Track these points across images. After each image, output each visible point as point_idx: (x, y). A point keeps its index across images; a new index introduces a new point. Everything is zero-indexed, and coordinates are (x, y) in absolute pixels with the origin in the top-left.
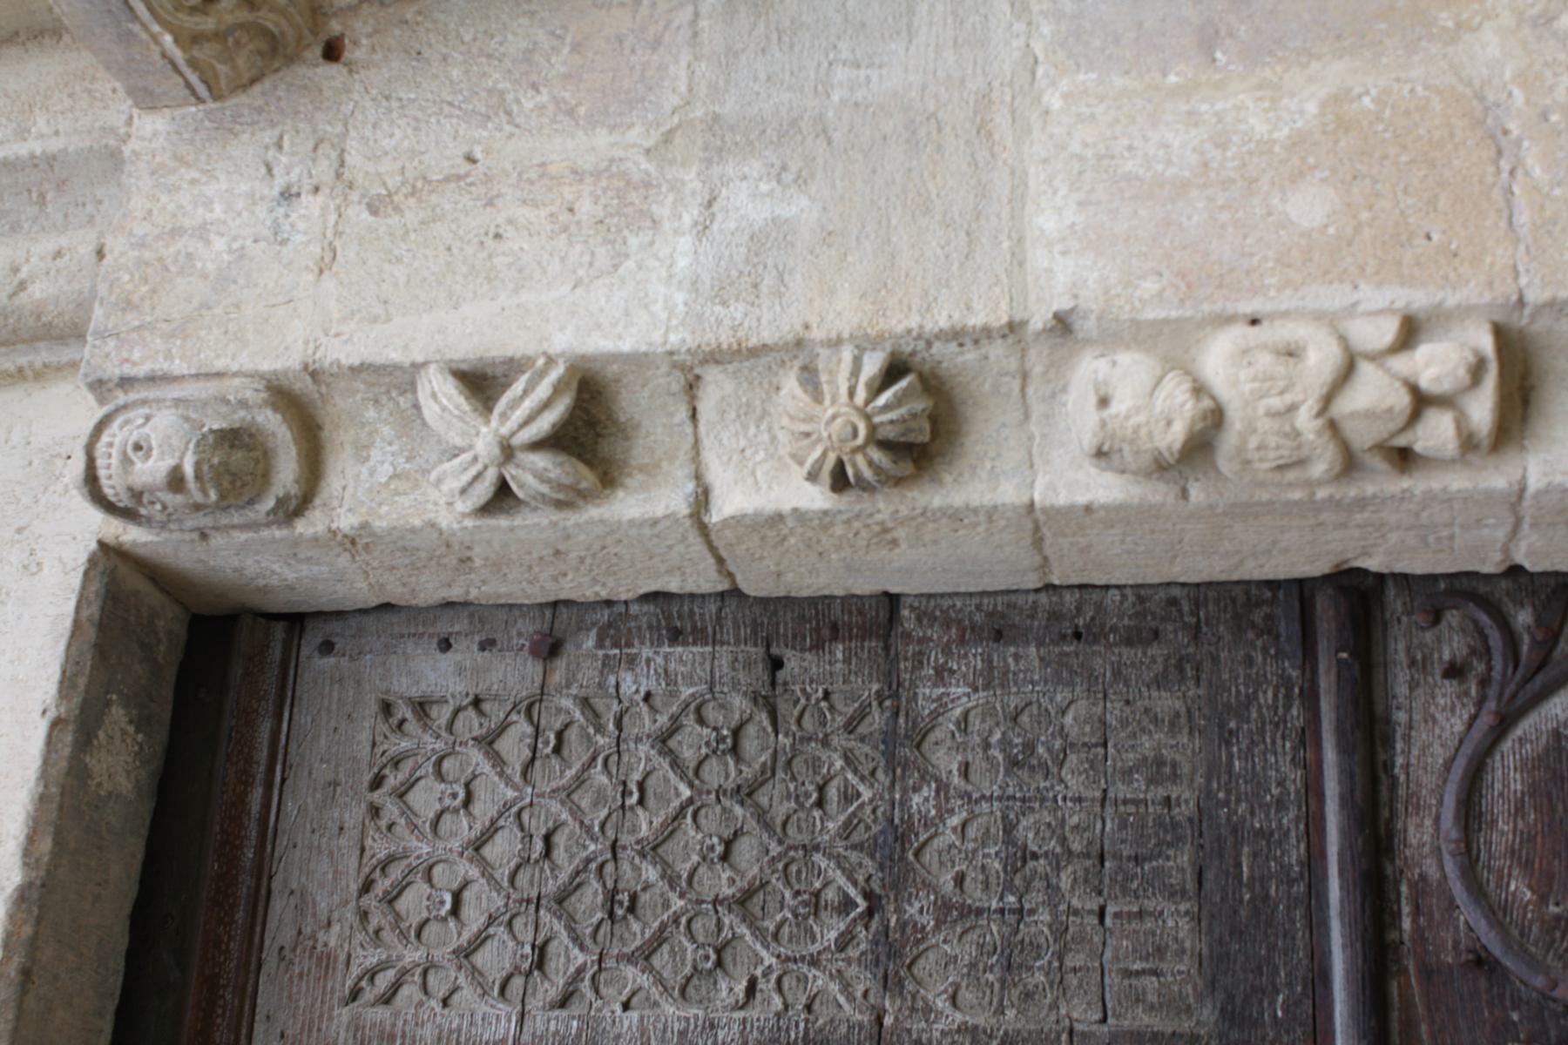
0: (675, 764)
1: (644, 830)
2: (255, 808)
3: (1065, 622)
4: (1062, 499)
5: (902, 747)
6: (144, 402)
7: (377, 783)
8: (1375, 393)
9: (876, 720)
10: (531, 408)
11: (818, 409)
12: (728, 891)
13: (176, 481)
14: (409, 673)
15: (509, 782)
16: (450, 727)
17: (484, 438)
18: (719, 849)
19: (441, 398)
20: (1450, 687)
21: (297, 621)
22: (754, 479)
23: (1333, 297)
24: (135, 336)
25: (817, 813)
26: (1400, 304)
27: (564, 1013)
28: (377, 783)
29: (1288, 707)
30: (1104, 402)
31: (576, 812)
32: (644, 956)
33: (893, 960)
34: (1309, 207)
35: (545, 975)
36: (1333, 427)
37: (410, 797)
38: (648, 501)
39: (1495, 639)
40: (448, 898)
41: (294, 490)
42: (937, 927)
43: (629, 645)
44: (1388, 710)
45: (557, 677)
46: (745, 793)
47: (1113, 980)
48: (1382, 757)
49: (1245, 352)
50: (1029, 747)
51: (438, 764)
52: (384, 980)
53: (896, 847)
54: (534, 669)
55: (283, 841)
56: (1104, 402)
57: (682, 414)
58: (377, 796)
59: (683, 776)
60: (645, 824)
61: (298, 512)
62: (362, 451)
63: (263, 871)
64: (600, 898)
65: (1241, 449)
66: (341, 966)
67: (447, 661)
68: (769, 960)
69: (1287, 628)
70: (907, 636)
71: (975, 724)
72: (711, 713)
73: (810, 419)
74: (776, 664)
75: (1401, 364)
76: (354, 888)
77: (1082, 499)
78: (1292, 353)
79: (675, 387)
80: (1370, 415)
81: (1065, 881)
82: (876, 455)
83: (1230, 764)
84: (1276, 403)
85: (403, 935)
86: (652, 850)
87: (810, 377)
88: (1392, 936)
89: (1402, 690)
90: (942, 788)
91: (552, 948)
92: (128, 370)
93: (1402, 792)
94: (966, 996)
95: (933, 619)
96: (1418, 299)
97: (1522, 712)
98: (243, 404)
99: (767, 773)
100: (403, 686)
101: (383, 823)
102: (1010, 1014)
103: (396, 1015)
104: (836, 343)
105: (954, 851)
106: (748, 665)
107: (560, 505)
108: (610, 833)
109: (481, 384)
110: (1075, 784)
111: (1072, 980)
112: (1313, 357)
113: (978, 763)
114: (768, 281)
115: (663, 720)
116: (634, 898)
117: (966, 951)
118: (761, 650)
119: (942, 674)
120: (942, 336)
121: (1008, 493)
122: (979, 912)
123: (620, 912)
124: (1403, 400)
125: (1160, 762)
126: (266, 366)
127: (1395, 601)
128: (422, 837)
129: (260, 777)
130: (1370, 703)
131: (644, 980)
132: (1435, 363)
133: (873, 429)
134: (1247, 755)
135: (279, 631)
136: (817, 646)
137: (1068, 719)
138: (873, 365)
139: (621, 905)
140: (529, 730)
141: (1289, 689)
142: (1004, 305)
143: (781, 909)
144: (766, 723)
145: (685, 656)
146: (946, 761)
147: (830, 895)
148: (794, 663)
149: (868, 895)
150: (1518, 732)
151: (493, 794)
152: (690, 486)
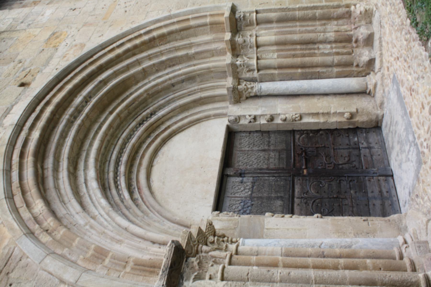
3: (278, 132)
8: (294, 117)
10: (252, 117)
17: (250, 118)
21: (235, 132)
33: (269, 146)
34: (291, 110)
38: (258, 123)
53: (269, 142)
105: (272, 142)
109: (250, 116)
139: (254, 145)
143: (263, 144)
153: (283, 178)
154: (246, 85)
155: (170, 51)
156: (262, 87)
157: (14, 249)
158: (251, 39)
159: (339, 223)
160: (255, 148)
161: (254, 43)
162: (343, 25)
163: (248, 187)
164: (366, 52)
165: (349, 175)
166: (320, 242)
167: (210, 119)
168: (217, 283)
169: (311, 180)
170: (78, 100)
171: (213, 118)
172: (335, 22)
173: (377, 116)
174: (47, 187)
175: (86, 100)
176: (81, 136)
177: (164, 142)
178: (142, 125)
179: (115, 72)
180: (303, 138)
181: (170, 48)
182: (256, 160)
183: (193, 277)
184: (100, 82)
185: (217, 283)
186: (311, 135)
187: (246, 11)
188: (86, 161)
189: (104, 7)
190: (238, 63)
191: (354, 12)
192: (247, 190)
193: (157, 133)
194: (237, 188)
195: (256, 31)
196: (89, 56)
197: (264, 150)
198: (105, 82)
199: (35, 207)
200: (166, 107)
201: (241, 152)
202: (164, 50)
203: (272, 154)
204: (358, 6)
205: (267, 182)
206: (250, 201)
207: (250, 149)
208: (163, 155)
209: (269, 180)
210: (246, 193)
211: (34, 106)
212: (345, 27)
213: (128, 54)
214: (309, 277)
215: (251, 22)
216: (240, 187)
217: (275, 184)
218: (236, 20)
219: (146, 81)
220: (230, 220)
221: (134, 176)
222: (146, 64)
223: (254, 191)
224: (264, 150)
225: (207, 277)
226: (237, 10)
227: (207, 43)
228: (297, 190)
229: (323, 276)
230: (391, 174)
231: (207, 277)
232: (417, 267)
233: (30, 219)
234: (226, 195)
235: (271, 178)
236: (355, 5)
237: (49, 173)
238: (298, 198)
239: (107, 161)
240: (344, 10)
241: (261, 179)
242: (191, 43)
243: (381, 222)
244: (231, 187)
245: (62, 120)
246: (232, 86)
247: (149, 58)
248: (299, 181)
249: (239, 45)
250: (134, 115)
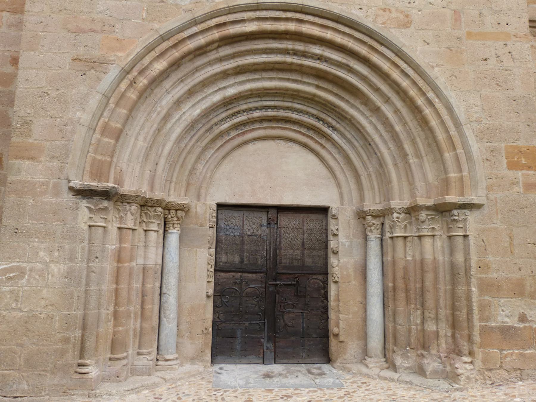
8: (335, 275)
10: (336, 232)
33: (309, 249)
109: (337, 230)
154: (374, 224)
155: (409, 133)
156: (373, 242)
157: (114, 64)
158: (426, 230)
161: (422, 234)
162: (446, 343)
163: (255, 231)
164: (409, 363)
165: (266, 324)
166: (171, 294)
168: (86, 223)
170: (316, 50)
172: (449, 334)
173: (335, 361)
174: (195, 61)
175: (320, 58)
176: (277, 66)
177: (305, 146)
178: (317, 120)
179: (366, 77)
180: (319, 283)
181: (412, 133)
182: (291, 237)
183: (89, 205)
184: (348, 66)
185: (86, 223)
186: (323, 291)
187: (468, 223)
188: (249, 81)
189: (503, 24)
190: (395, 215)
191: (460, 360)
193: (315, 137)
195: (440, 235)
196: (382, 42)
197: (303, 244)
198: (350, 70)
199: (159, 63)
200: (344, 141)
201: (301, 222)
202: (409, 126)
203: (299, 252)
204: (468, 367)
207: (305, 231)
208: (288, 147)
209: (263, 250)
210: (249, 230)
211: (291, 9)
212: (444, 346)
213: (395, 86)
214: (90, 286)
215: (451, 229)
218: (451, 211)
219: (368, 113)
220: (205, 220)
221: (256, 126)
222: (385, 109)
225: (91, 215)
226: (470, 211)
227: (424, 176)
228: (250, 275)
229: (90, 296)
230: (265, 362)
231: (91, 215)
232: (113, 362)
233: (143, 65)
235: (265, 252)
236: (472, 363)
237: (213, 56)
238: (241, 276)
239: (260, 97)
240: (465, 346)
242: (422, 158)
243: (201, 345)
245: (285, 42)
246: (367, 209)
247: (397, 111)
249: (418, 216)
250: (326, 110)
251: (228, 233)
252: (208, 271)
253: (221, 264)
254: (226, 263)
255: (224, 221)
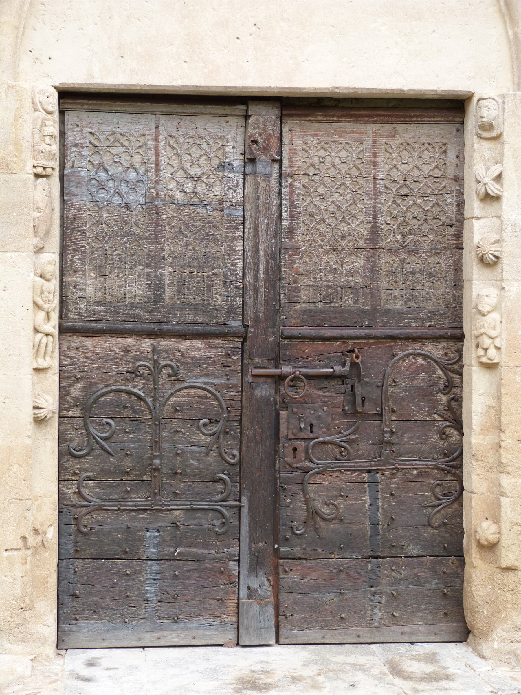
0: (432, 207)
1: (418, 201)
2: (424, 119)
4: (474, 286)
5: (435, 252)
6: (499, 108)
7: (429, 144)
8: (486, 342)
9: (439, 246)
10: (493, 189)
11: (489, 244)
12: (407, 218)
13: (482, 117)
14: (452, 149)
15: (429, 172)
16: (440, 158)
18: (415, 216)
19: (496, 170)
20: (443, 353)
21: (463, 123)
22: (479, 231)
23: (504, 335)
24: (514, 103)
25: (422, 235)
26: (502, 347)
27: (384, 188)
28: (429, 144)
29: (440, 324)
30: (487, 296)
31: (423, 187)
32: (394, 202)
33: (394, 251)
35: (391, 183)
36: (482, 335)
37: (426, 151)
39: (450, 362)
40: (406, 162)
41: (482, 136)
42: (400, 259)
43: (456, 196)
44: (439, 342)
45: (450, 181)
46: (426, 220)
47: (390, 291)
48: (430, 340)
49: (495, 321)
50: (434, 276)
51: (433, 157)
52: (390, 150)
53: (415, 251)
54: (452, 176)
55: (417, 125)
56: (487, 296)
57: (494, 215)
58: (426, 144)
59: (429, 208)
60: (420, 201)
61: (478, 136)
62: (490, 149)
63: (412, 122)
64: (406, 193)
65: (479, 319)
66: (392, 141)
67: (454, 157)
68: (394, 227)
69: (455, 324)
70: (456, 252)
71: (438, 265)
72: (442, 213)
73: (488, 242)
74: (451, 226)
75: (492, 346)
76: (408, 142)
77: (473, 290)
78: (494, 328)
79: (498, 214)
80: (483, 341)
81: (408, 283)
82: (481, 254)
83: (429, 313)
84: (486, 325)
85: (399, 153)
86: (415, 203)
87: (497, 242)
88: (398, 341)
89: (443, 344)
90: (426, 259)
91: (396, 184)
92: (506, 103)
93: (424, 343)
94: (387, 264)
95: (459, 257)
96: (503, 350)
97: (438, 365)
98: (497, 129)
99: (430, 225)
100: (449, 148)
101: (421, 146)
102: (384, 273)
103: (383, 153)
104: (502, 247)
105: (415, 262)
106: (451, 220)
107: (476, 192)
108: (418, 194)
109: (499, 178)
110: (427, 284)
111: (390, 284)
112: (493, 332)
113: (431, 266)
114: (515, 234)
115: (441, 204)
116: (406, 200)
117: (395, 265)
118: (454, 223)
119: (448, 259)
120: (502, 267)
121: (475, 277)
122: (403, 267)
123: (403, 197)
124: (485, 347)
125: (431, 300)
126: (505, 133)
127: (459, 344)
128: (418, 155)
129: (430, 119)
130: (317, 339)
131: (390, 203)
132: (492, 353)
133: (485, 254)
134: (431, 316)
135: (461, 120)
136: (455, 234)
137: (439, 283)
138: (496, 254)
139: (404, 197)
140: (439, 176)
141: (443, 324)
142: (507, 278)
144: (440, 224)
145: (454, 208)
146: (431, 260)
147: (406, 238)
148: (452, 229)
149: (406, 246)
150: (435, 364)
151: (426, 169)
152: (480, 216)
153: (239, 300)
159: (15, 468)
160: (384, 203)
163: (201, 188)
165: (245, 511)
167: (505, 22)
169: (227, 393)
171: (511, 33)
192: (188, 186)
194: (196, 153)
197: (374, 233)
201: (368, 152)
203: (360, 262)
205: (222, 248)
206: (142, 200)
207: (381, 185)
209: (232, 256)
210: (180, 185)
216: (203, 161)
217: (216, 275)
223: (186, 212)
224: (374, 233)
234: (163, 119)
235: (240, 262)
238: (154, 350)
241: (236, 230)
244: (201, 132)
248: (223, 352)
251: (102, 195)
252: (36, 331)
253: (83, 306)
254: (99, 303)
255: (86, 152)
